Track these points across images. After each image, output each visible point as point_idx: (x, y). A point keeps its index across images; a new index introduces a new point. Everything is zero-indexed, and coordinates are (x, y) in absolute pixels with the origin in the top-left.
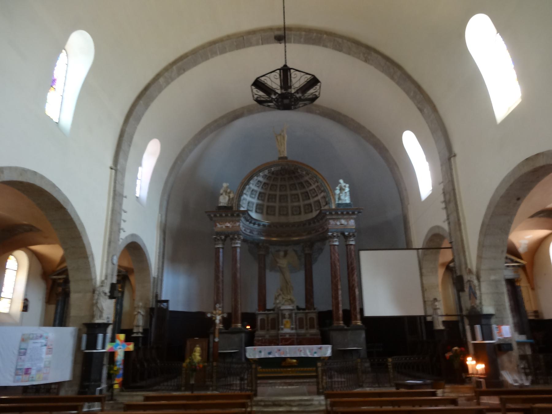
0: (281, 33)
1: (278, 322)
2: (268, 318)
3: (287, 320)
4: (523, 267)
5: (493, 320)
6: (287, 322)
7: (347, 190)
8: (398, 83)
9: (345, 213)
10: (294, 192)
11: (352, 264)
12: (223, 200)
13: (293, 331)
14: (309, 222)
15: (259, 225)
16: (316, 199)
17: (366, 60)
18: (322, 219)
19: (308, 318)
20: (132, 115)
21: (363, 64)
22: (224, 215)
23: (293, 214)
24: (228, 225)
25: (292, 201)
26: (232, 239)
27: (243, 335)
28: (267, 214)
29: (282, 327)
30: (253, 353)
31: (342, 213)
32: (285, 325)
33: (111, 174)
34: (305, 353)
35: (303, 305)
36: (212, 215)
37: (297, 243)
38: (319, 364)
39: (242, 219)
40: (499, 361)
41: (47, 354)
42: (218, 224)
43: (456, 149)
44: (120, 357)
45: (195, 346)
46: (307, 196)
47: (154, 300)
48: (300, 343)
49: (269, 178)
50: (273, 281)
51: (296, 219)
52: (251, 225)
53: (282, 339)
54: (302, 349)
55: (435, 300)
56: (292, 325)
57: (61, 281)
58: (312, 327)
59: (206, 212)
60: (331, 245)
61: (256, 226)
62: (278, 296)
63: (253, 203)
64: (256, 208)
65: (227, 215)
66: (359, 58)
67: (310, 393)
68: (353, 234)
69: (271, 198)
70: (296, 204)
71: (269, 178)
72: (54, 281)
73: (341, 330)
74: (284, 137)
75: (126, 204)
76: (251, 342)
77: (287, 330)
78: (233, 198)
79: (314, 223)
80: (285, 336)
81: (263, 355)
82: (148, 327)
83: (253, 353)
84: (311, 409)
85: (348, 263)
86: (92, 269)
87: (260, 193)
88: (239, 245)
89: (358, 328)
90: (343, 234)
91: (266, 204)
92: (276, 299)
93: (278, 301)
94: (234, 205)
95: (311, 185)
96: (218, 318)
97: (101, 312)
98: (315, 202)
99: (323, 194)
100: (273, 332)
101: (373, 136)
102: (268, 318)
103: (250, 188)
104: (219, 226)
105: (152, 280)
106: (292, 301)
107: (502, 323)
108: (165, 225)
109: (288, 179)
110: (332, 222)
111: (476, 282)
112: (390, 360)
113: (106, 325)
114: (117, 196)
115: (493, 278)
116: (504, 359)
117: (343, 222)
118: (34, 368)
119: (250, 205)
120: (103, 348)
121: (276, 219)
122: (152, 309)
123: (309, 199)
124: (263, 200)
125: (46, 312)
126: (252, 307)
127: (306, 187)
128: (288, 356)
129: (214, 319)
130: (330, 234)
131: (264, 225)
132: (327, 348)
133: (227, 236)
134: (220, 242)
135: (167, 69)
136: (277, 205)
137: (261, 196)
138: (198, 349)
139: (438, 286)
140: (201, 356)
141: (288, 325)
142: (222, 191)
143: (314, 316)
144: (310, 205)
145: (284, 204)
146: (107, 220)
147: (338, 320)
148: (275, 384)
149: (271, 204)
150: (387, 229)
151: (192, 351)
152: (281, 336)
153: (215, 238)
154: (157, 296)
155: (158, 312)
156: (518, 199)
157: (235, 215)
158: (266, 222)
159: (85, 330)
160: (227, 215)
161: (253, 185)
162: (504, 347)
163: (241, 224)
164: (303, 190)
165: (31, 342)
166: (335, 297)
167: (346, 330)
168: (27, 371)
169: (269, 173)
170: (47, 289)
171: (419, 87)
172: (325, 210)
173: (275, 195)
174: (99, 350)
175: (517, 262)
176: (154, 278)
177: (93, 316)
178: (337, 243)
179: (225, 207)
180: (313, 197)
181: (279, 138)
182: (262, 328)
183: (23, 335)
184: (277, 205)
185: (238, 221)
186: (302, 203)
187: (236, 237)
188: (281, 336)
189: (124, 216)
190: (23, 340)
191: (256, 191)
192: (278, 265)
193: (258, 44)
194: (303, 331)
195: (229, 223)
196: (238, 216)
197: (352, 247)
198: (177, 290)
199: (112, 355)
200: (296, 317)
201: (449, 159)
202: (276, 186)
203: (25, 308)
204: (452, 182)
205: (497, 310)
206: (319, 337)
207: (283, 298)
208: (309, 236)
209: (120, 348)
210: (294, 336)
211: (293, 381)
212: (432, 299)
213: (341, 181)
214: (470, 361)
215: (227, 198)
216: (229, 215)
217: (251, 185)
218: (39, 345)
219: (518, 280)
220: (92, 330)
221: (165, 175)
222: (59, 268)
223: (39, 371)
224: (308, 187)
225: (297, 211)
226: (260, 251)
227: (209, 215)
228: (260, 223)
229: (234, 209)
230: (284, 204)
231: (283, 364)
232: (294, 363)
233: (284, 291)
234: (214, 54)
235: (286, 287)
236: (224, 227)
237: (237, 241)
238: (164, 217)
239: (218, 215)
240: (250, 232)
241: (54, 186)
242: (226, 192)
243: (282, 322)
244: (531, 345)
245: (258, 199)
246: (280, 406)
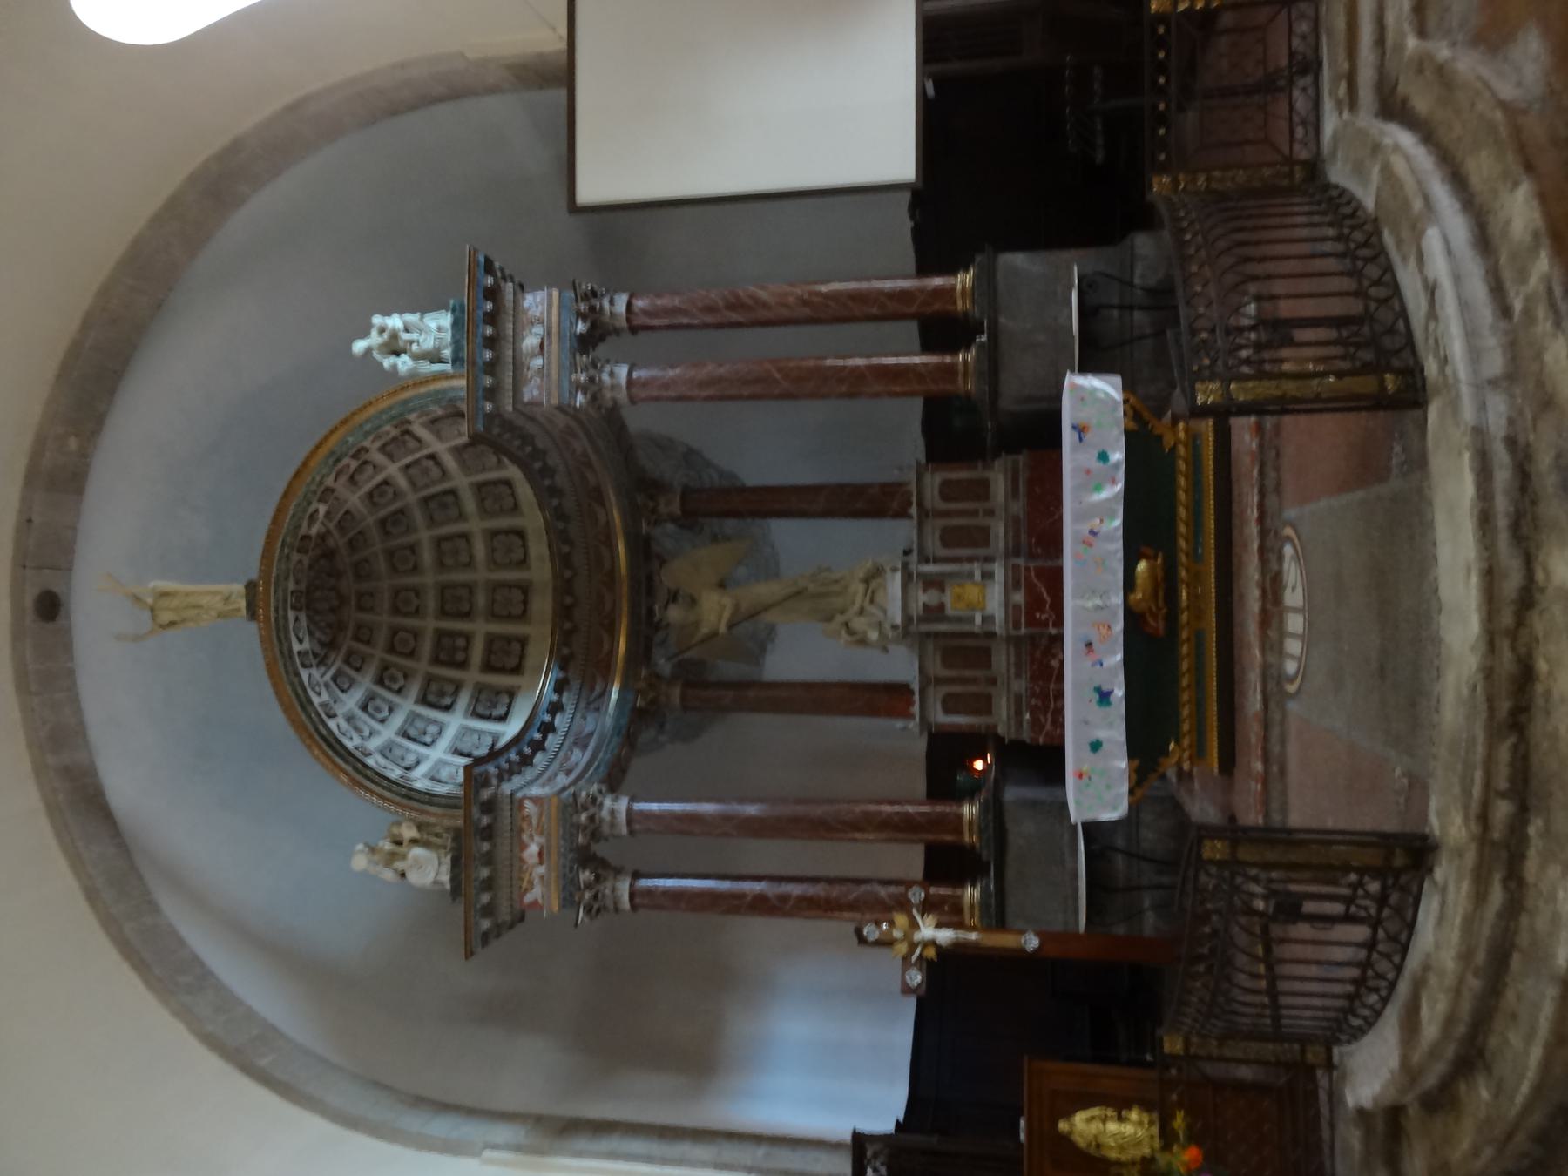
1: (953, 635)
2: (940, 681)
3: (948, 598)
6: (959, 598)
7: (395, 322)
9: (489, 331)
10: (427, 556)
11: (710, 309)
12: (428, 868)
13: (998, 570)
14: (547, 494)
15: (555, 708)
16: (450, 462)
18: (526, 439)
19: (943, 506)
23: (523, 563)
24: (533, 849)
25: (470, 564)
26: (595, 835)
27: (1011, 794)
28: (517, 670)
29: (978, 620)
31: (491, 343)
32: (972, 607)
34: (1103, 511)
36: (486, 924)
37: (643, 550)
42: (528, 898)
45: (1066, 1140)
48: (1051, 541)
52: (552, 741)
53: (1031, 621)
54: (1085, 528)
56: (971, 575)
58: (980, 490)
59: (469, 954)
60: (633, 400)
61: (560, 721)
62: (851, 632)
64: (488, 718)
68: (585, 297)
69: (450, 653)
71: (355, 662)
74: (165, 595)
77: (989, 599)
78: (420, 827)
79: (547, 471)
80: (1017, 607)
81: (1114, 732)
85: (706, 326)
87: (424, 700)
91: (473, 676)
94: (447, 822)
95: (386, 483)
96: (928, 930)
100: (1001, 660)
102: (940, 681)
103: (387, 751)
104: (535, 894)
106: (875, 575)
109: (349, 587)
110: (531, 392)
117: (530, 341)
121: (539, 633)
123: (453, 492)
126: (904, 739)
127: (398, 505)
128: (1117, 599)
129: (931, 953)
130: (580, 399)
131: (559, 687)
132: (1082, 396)
133: (586, 858)
137: (437, 697)
138: (1084, 1125)
140: (1120, 1105)
141: (972, 592)
145: (481, 600)
148: (1273, 679)
152: (1017, 625)
153: (588, 910)
157: (485, 820)
160: (489, 859)
161: (376, 740)
163: (535, 791)
164: (418, 516)
166: (855, 384)
167: (994, 337)
169: (322, 662)
173: (440, 634)
178: (622, 371)
179: (455, 863)
180: (445, 473)
181: (166, 617)
182: (983, 704)
184: (480, 628)
185: (516, 803)
186: (476, 526)
187: (583, 817)
188: (1017, 625)
192: (723, 629)
194: (999, 529)
195: (524, 847)
197: (639, 304)
200: (936, 560)
202: (394, 632)
206: (1022, 459)
207: (861, 612)
208: (612, 497)
210: (1016, 568)
211: (1251, 572)
213: (359, 346)
215: (417, 851)
216: (486, 846)
224: (397, 494)
226: (681, 692)
227: (486, 938)
228: (545, 704)
230: (481, 600)
231: (1158, 625)
232: (1152, 570)
233: (846, 607)
235: (819, 600)
236: (541, 870)
237: (605, 814)
238: (504, 1133)
239: (485, 898)
240: (584, 747)
242: (391, 858)
243: (959, 620)
245: (448, 708)
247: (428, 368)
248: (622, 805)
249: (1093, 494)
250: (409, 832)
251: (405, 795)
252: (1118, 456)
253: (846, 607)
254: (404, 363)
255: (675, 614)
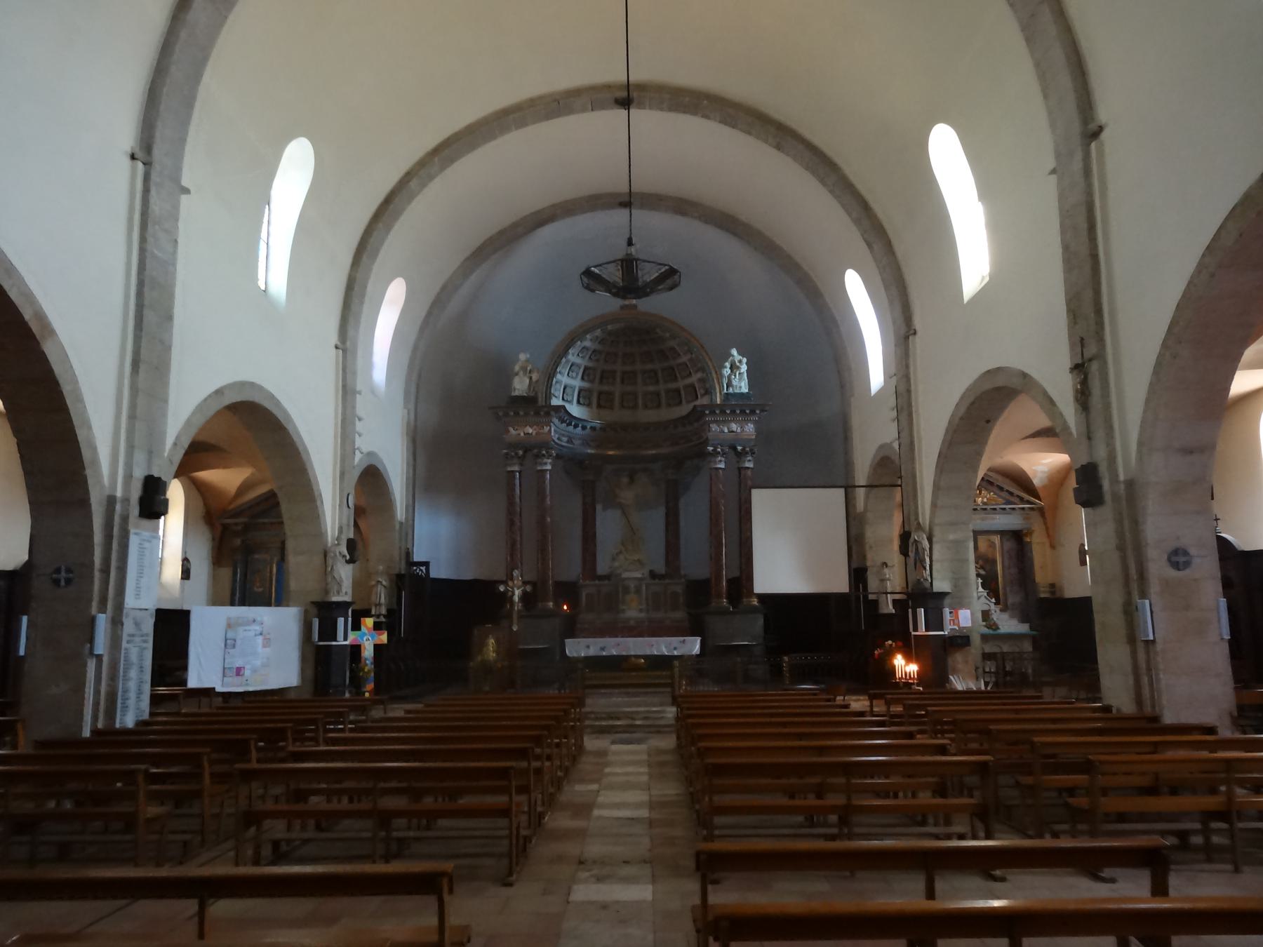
0: (627, 199)
4: (1041, 511)
5: (947, 601)
7: (744, 368)
8: (831, 192)
10: (649, 366)
12: (520, 386)
13: (643, 615)
14: (676, 422)
15: (584, 428)
17: (778, 147)
20: (364, 251)
21: (775, 152)
22: (521, 413)
24: (530, 431)
26: (538, 456)
28: (599, 406)
30: (577, 648)
31: (733, 412)
33: (337, 356)
35: (660, 568)
36: (501, 414)
37: (654, 459)
38: (676, 663)
39: (556, 421)
40: (950, 661)
41: (264, 646)
43: (918, 323)
44: (368, 652)
46: (672, 374)
47: (403, 562)
49: (602, 342)
50: (608, 525)
51: (650, 416)
55: (885, 564)
57: (239, 528)
63: (573, 388)
65: (526, 414)
66: (766, 141)
67: (661, 705)
69: (605, 376)
70: (651, 388)
71: (602, 342)
72: (225, 527)
73: (724, 612)
75: (362, 405)
76: (572, 628)
77: (633, 611)
81: (592, 652)
82: (395, 607)
83: (577, 648)
84: (662, 722)
86: (81, 435)
87: (586, 369)
88: (549, 467)
89: (754, 610)
90: (734, 448)
92: (614, 559)
93: (616, 564)
97: (340, 585)
98: (686, 387)
99: (699, 375)
101: (797, 266)
103: (567, 361)
105: (397, 527)
107: (960, 603)
108: (416, 426)
110: (714, 427)
111: (926, 544)
112: (786, 658)
113: (345, 605)
114: (347, 393)
115: (951, 537)
116: (958, 659)
117: (734, 426)
118: (247, 667)
119: (568, 390)
120: (345, 639)
122: (400, 577)
124: (592, 381)
125: (215, 579)
126: (569, 567)
130: (711, 448)
131: (593, 429)
134: (515, 461)
135: (423, 163)
136: (617, 389)
137: (587, 374)
138: (491, 641)
139: (891, 541)
142: (517, 368)
143: (679, 589)
144: (678, 391)
146: (335, 437)
147: (719, 596)
149: (605, 388)
150: (808, 441)
151: (483, 644)
154: (408, 554)
155: (412, 581)
156: (988, 421)
158: (597, 423)
159: (314, 611)
160: (526, 414)
161: (572, 356)
162: (960, 641)
165: (241, 629)
166: (716, 558)
168: (239, 671)
170: (213, 539)
171: (865, 206)
172: (703, 406)
173: (614, 372)
174: (341, 641)
175: (1029, 502)
176: (401, 523)
177: (327, 592)
178: (722, 466)
180: (683, 378)
183: (229, 619)
189: (359, 426)
190: (229, 626)
191: (579, 366)
193: (584, 110)
196: (548, 414)
197: (749, 472)
198: (439, 541)
199: (356, 649)
201: (907, 338)
203: (186, 574)
204: (907, 377)
205: (955, 586)
209: (368, 639)
212: (879, 563)
213: (734, 352)
214: (899, 661)
215: (528, 381)
217: (570, 357)
218: (252, 633)
219: (1030, 533)
220: (324, 614)
221: (412, 338)
222: (232, 506)
223: (254, 671)
225: (655, 401)
229: (541, 402)
233: (627, 543)
234: (504, 129)
241: (272, 397)
244: (1035, 641)
245: (583, 378)
246: (619, 719)
247: (725, 382)
248: (549, 467)
249: (663, 646)
250: (535, 376)
251: (550, 375)
252: (676, 653)
253: (627, 543)
254: (727, 371)
255: (625, 480)
